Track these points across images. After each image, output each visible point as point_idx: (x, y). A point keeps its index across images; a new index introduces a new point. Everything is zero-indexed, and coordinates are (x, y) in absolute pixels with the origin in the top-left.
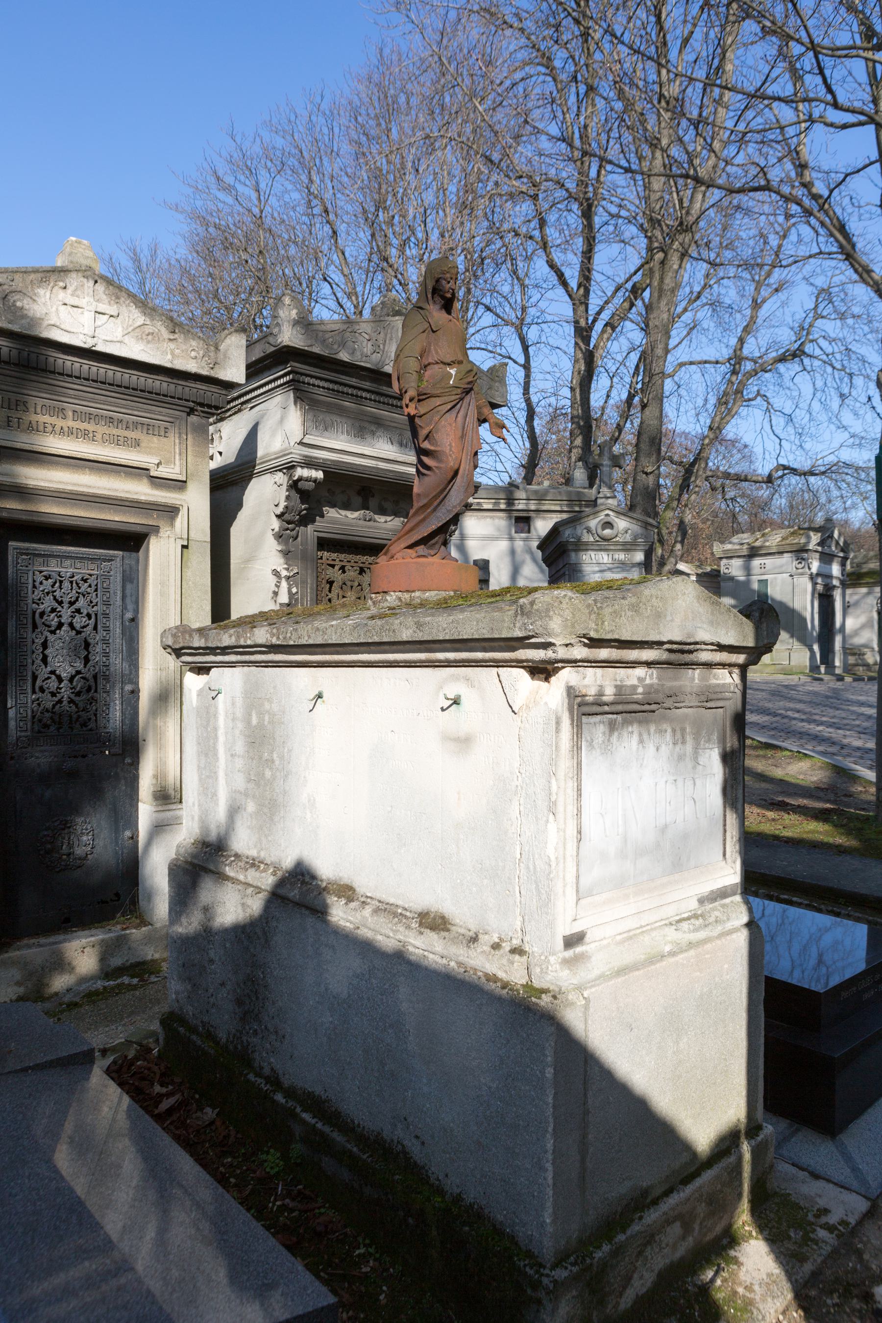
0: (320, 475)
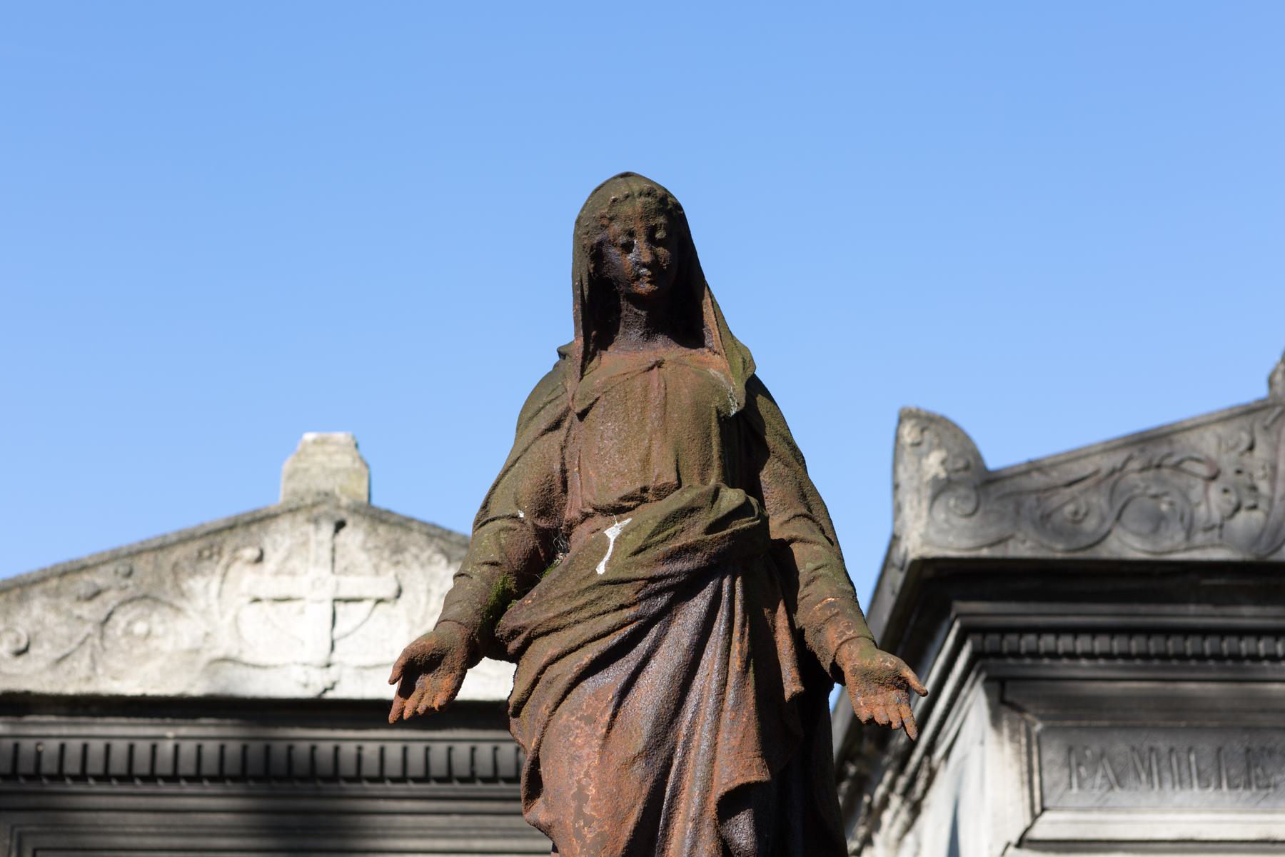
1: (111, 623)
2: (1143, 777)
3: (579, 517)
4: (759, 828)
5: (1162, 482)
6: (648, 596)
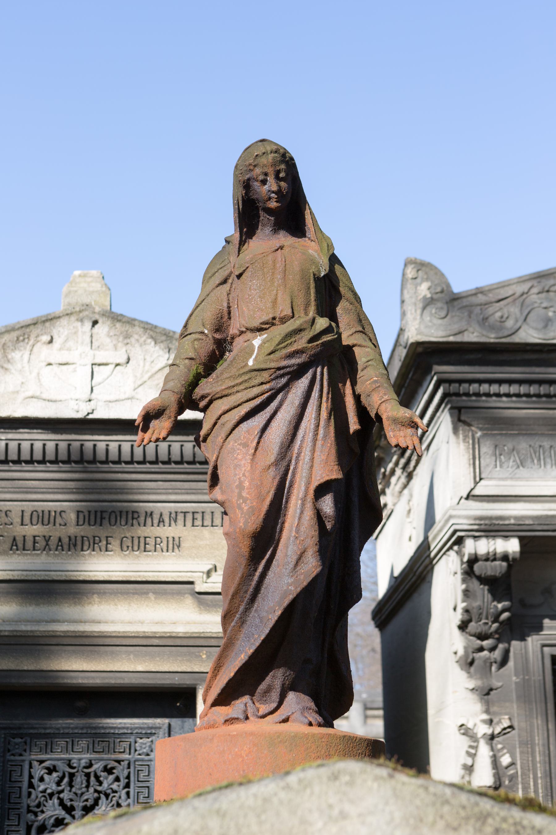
0: (512, 546)
2: (536, 461)
3: (238, 333)
4: (336, 502)
5: (550, 300)
6: (277, 378)
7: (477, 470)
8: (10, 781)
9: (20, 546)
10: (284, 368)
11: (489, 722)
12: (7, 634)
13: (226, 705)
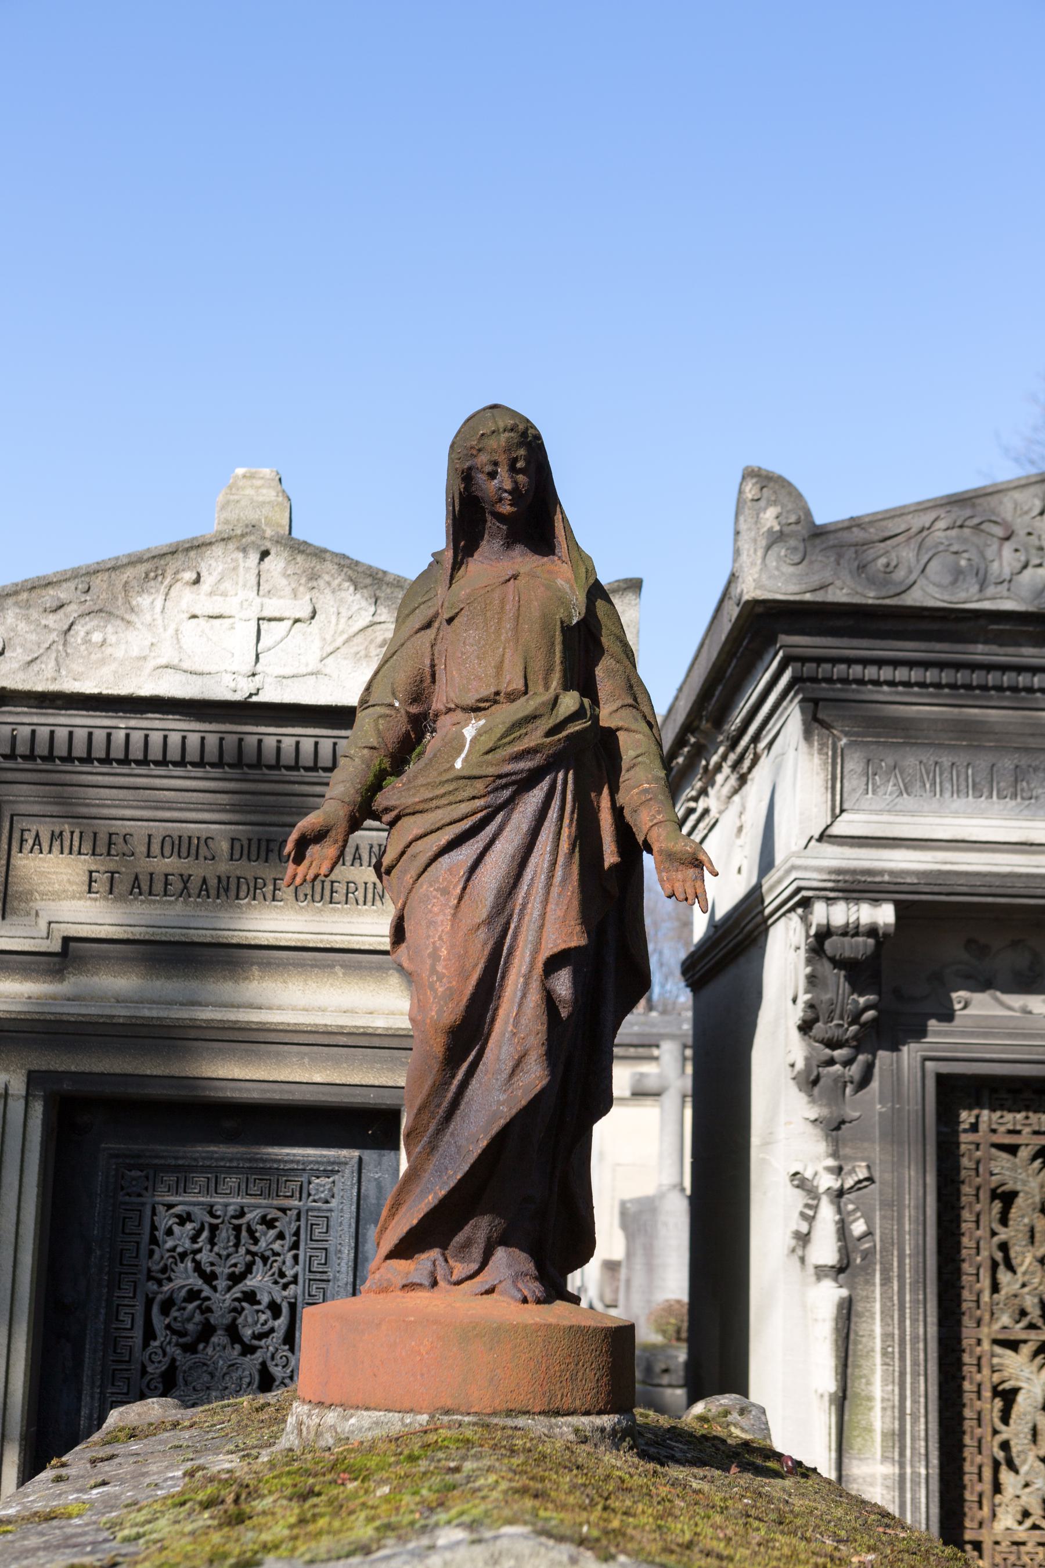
0: (885, 915)
1: (72, 632)
5: (964, 541)
7: (838, 797)
8: (123, 1232)
9: (145, 887)
10: (507, 775)
11: (837, 1171)
12: (121, 1021)
13: (407, 1259)
